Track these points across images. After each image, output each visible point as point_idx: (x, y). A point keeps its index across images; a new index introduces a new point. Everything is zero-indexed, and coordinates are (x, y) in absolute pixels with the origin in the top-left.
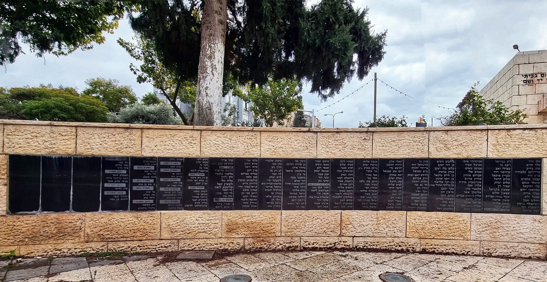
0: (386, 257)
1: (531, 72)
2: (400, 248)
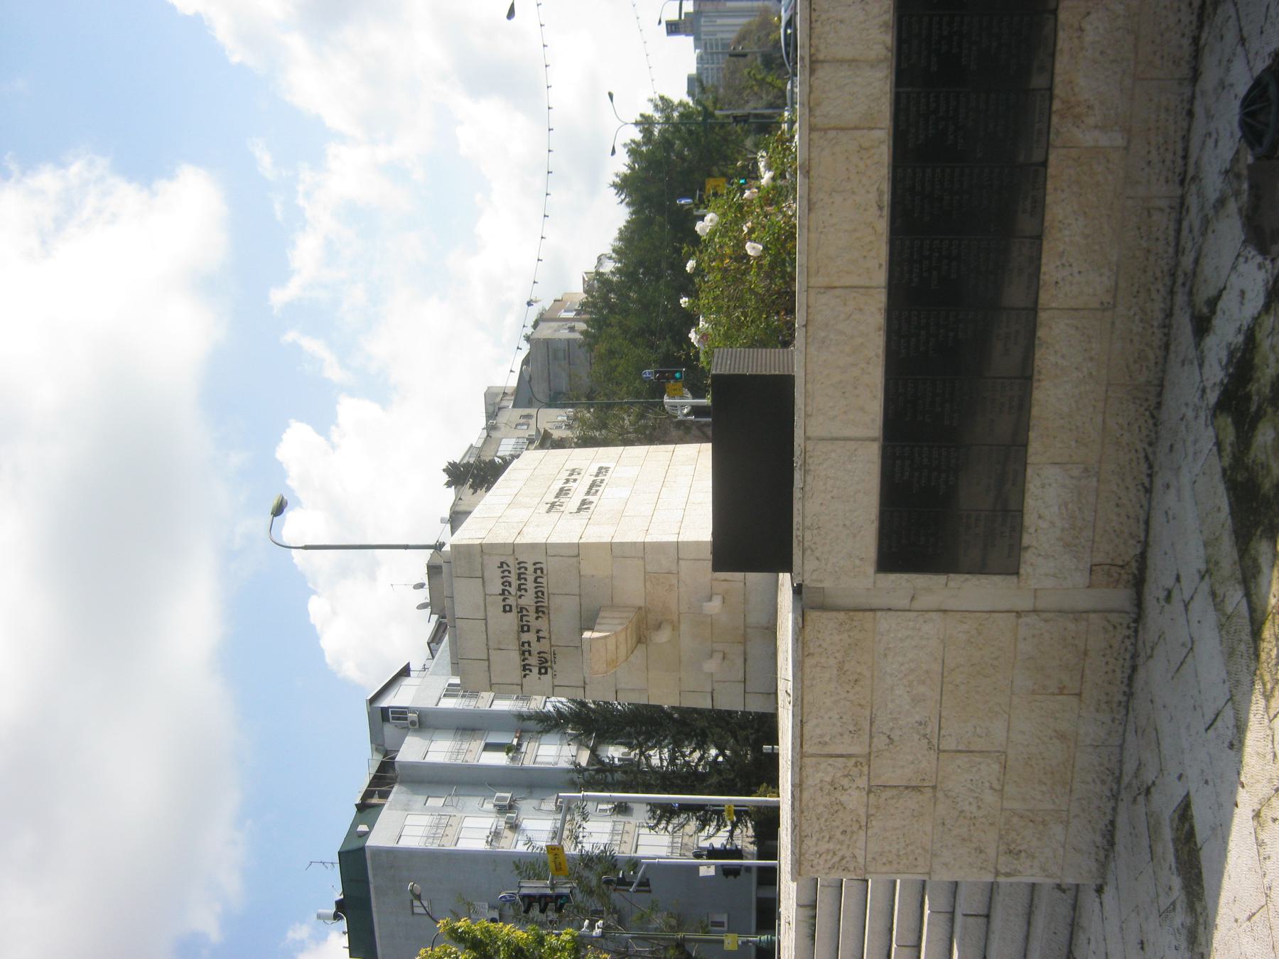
1: (515, 657)
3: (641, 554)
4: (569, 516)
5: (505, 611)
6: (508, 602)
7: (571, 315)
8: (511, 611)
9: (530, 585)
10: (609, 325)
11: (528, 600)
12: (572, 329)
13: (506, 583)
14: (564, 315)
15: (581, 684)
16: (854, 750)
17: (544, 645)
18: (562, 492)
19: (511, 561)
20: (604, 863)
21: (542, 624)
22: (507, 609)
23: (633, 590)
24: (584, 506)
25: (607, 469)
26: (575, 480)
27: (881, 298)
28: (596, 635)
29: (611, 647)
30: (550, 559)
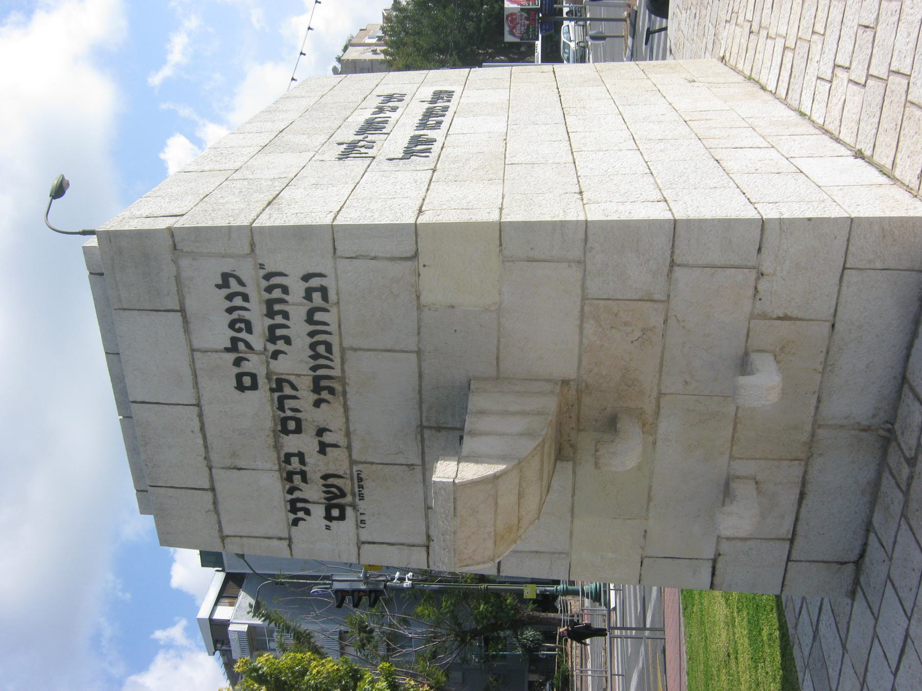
1: (271, 484)
3: (576, 253)
4: (387, 166)
5: (240, 387)
6: (246, 367)
7: (374, 41)
8: (254, 386)
9: (298, 328)
10: (405, 45)
11: (295, 363)
12: (374, 52)
13: (240, 324)
14: (368, 41)
15: (422, 539)
17: (336, 461)
18: (371, 126)
19: (246, 271)
21: (329, 416)
22: (245, 383)
23: (551, 339)
24: (417, 147)
25: (450, 94)
26: (394, 109)
28: (471, 471)
29: (507, 500)
30: (343, 264)
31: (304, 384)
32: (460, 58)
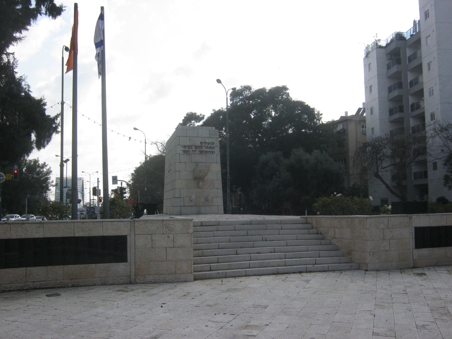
0: (49, 290)
1: (188, 144)
2: (60, 286)
5: (201, 142)
9: (208, 150)
11: (204, 149)
13: (208, 144)
16: (390, 226)
17: (191, 152)
20: (230, 175)
21: (197, 152)
27: (446, 225)
31: (201, 150)
32: (57, 202)
